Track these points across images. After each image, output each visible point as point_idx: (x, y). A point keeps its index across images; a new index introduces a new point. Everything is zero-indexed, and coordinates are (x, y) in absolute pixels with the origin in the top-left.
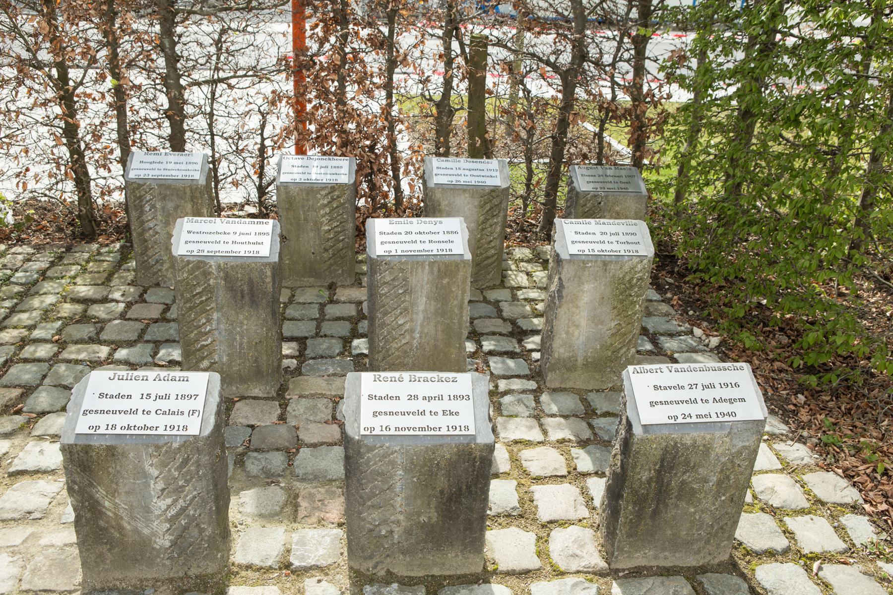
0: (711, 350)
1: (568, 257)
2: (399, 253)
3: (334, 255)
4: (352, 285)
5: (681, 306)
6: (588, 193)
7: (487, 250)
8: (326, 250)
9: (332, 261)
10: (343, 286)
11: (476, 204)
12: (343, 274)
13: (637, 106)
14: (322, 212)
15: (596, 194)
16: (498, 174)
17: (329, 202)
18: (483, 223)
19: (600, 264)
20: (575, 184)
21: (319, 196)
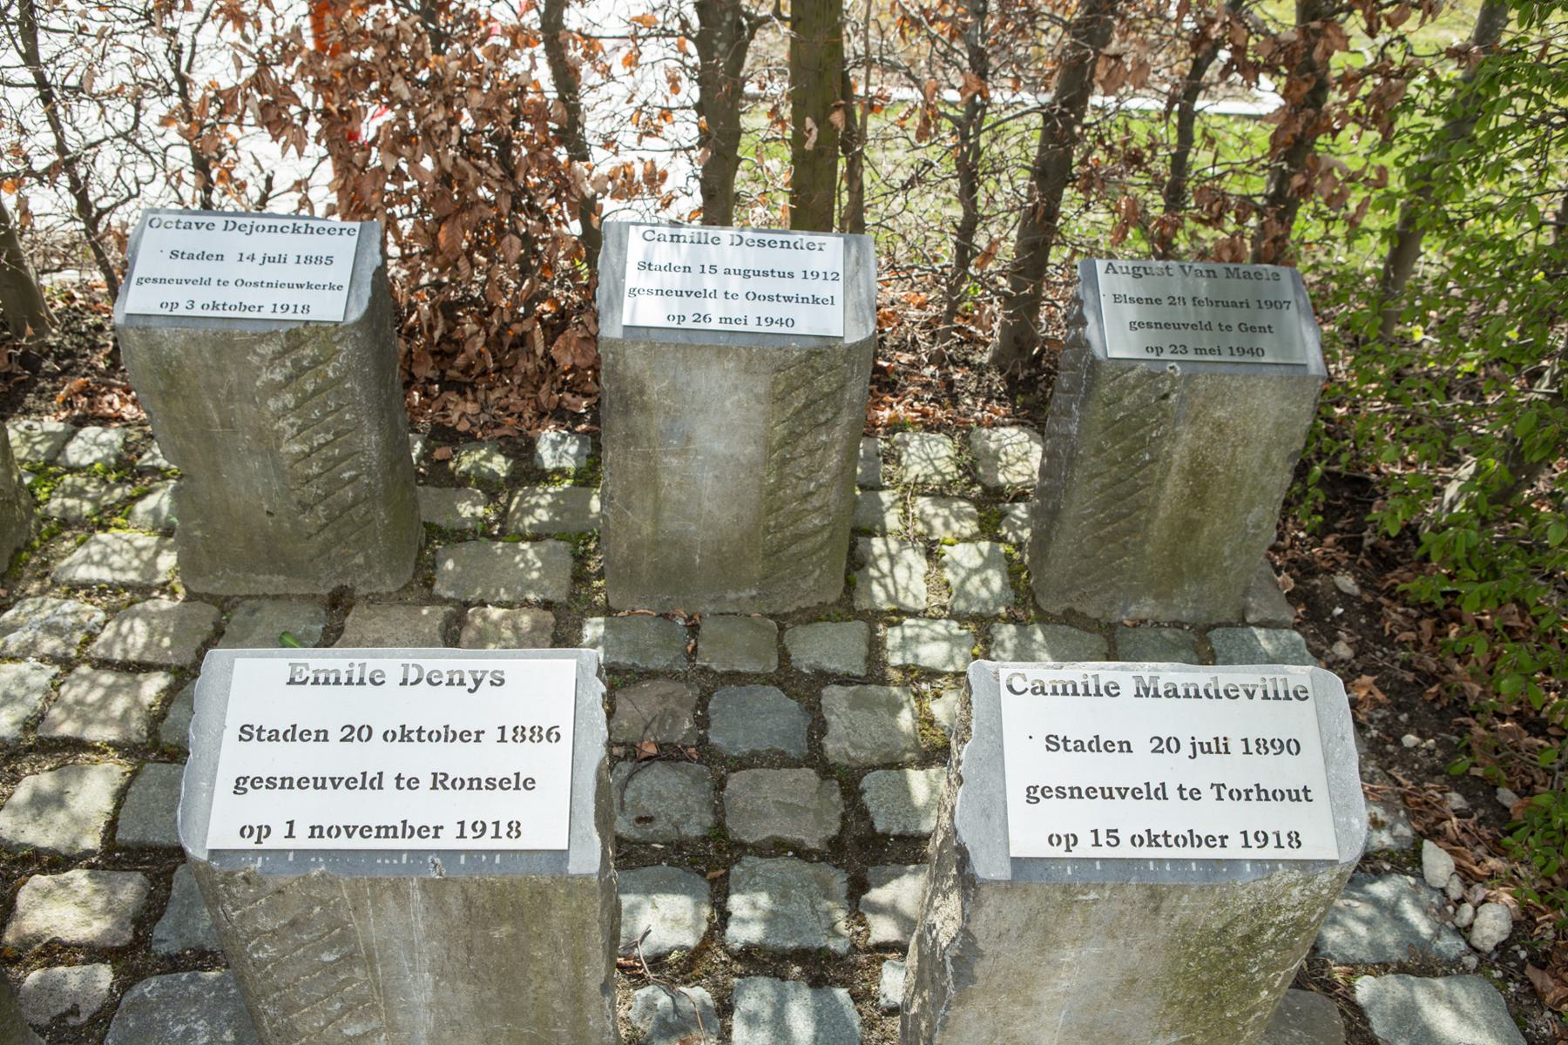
0: (1485, 961)
1: (1002, 872)
2: (302, 841)
3: (331, 519)
4: (398, 598)
5: (1378, 705)
6: (1130, 363)
7: (797, 517)
8: (305, 507)
9: (329, 534)
10: (373, 600)
11: (761, 390)
12: (368, 566)
13: (1318, 33)
14: (273, 404)
15: (1156, 369)
16: (837, 289)
17: (289, 379)
18: (783, 443)
19: (1134, 892)
20: (1091, 332)
21: (255, 360)
